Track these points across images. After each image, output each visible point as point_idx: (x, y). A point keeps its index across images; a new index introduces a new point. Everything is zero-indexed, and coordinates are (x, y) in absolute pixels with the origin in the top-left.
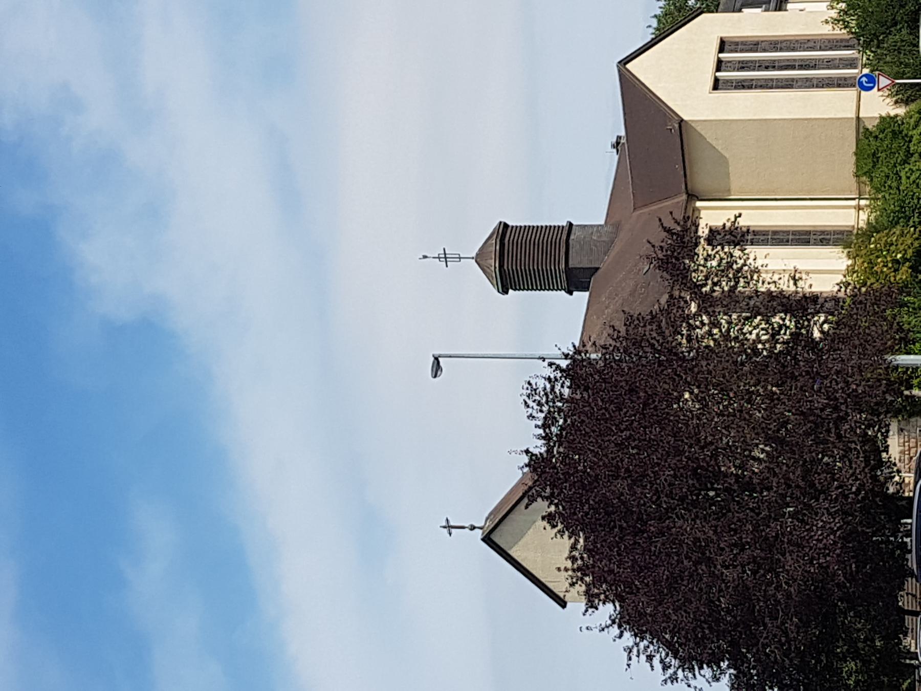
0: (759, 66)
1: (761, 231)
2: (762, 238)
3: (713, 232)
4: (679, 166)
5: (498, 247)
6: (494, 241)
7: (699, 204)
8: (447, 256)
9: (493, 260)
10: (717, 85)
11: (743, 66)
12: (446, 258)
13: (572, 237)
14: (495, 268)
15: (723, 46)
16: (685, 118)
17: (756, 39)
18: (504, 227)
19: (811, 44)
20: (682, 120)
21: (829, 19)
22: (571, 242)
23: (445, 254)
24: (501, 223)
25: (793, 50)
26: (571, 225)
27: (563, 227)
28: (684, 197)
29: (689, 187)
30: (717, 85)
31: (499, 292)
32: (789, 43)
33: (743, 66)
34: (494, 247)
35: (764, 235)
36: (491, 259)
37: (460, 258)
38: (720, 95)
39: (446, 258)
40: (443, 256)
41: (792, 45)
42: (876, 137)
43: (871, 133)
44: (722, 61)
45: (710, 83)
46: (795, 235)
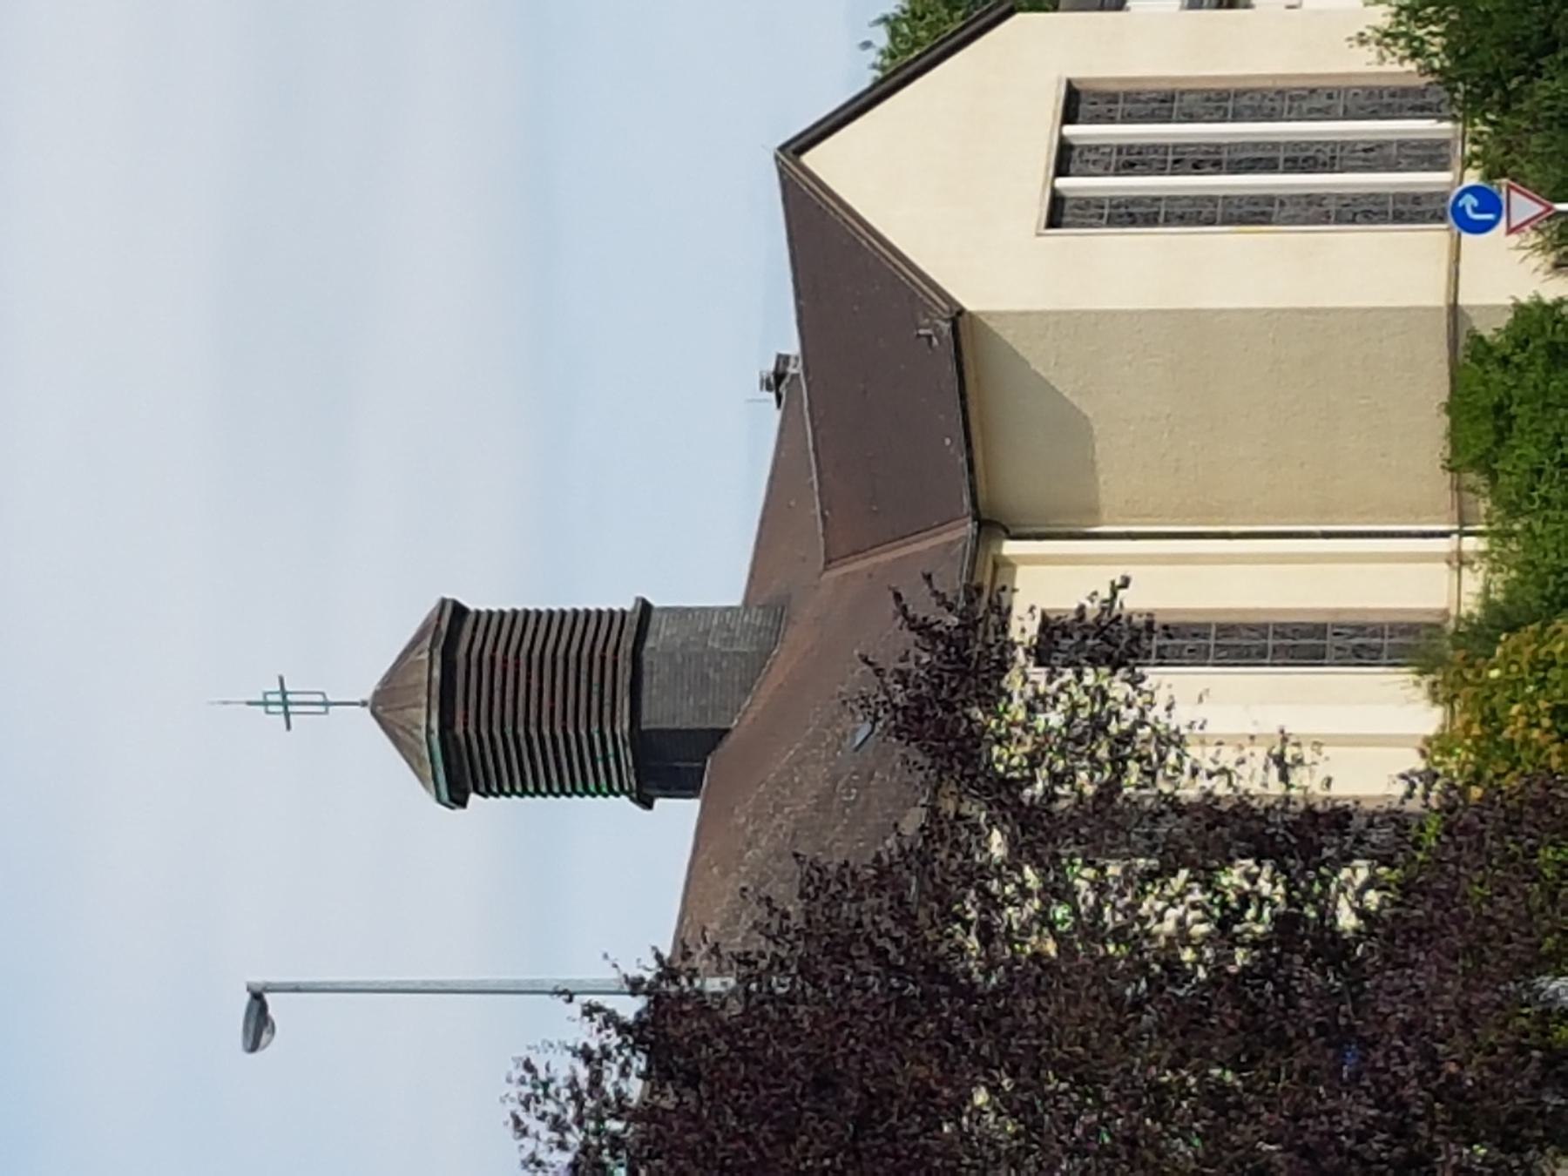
0: (1176, 162)
1: (1189, 626)
2: (1190, 643)
3: (1051, 628)
4: (951, 443)
5: (437, 673)
6: (425, 656)
7: (1010, 548)
8: (289, 697)
9: (424, 711)
10: (1058, 213)
11: (1131, 160)
12: (285, 704)
13: (649, 643)
14: (429, 731)
15: (1075, 104)
16: (970, 305)
17: (1167, 86)
18: (459, 611)
19: (1323, 102)
20: (958, 315)
21: (1369, 33)
22: (646, 657)
23: (284, 693)
24: (444, 602)
25: (1271, 117)
26: (645, 608)
27: (623, 613)
28: (970, 527)
29: (982, 498)
30: (1058, 213)
31: (439, 799)
32: (1258, 96)
33: (1131, 160)
34: (426, 672)
35: (1195, 635)
36: (417, 705)
37: (326, 704)
38: (1071, 241)
39: (285, 704)
40: (278, 698)
41: (1267, 103)
42: (1505, 361)
43: (1490, 349)
44: (1071, 147)
45: (1039, 209)
46: (1284, 636)
